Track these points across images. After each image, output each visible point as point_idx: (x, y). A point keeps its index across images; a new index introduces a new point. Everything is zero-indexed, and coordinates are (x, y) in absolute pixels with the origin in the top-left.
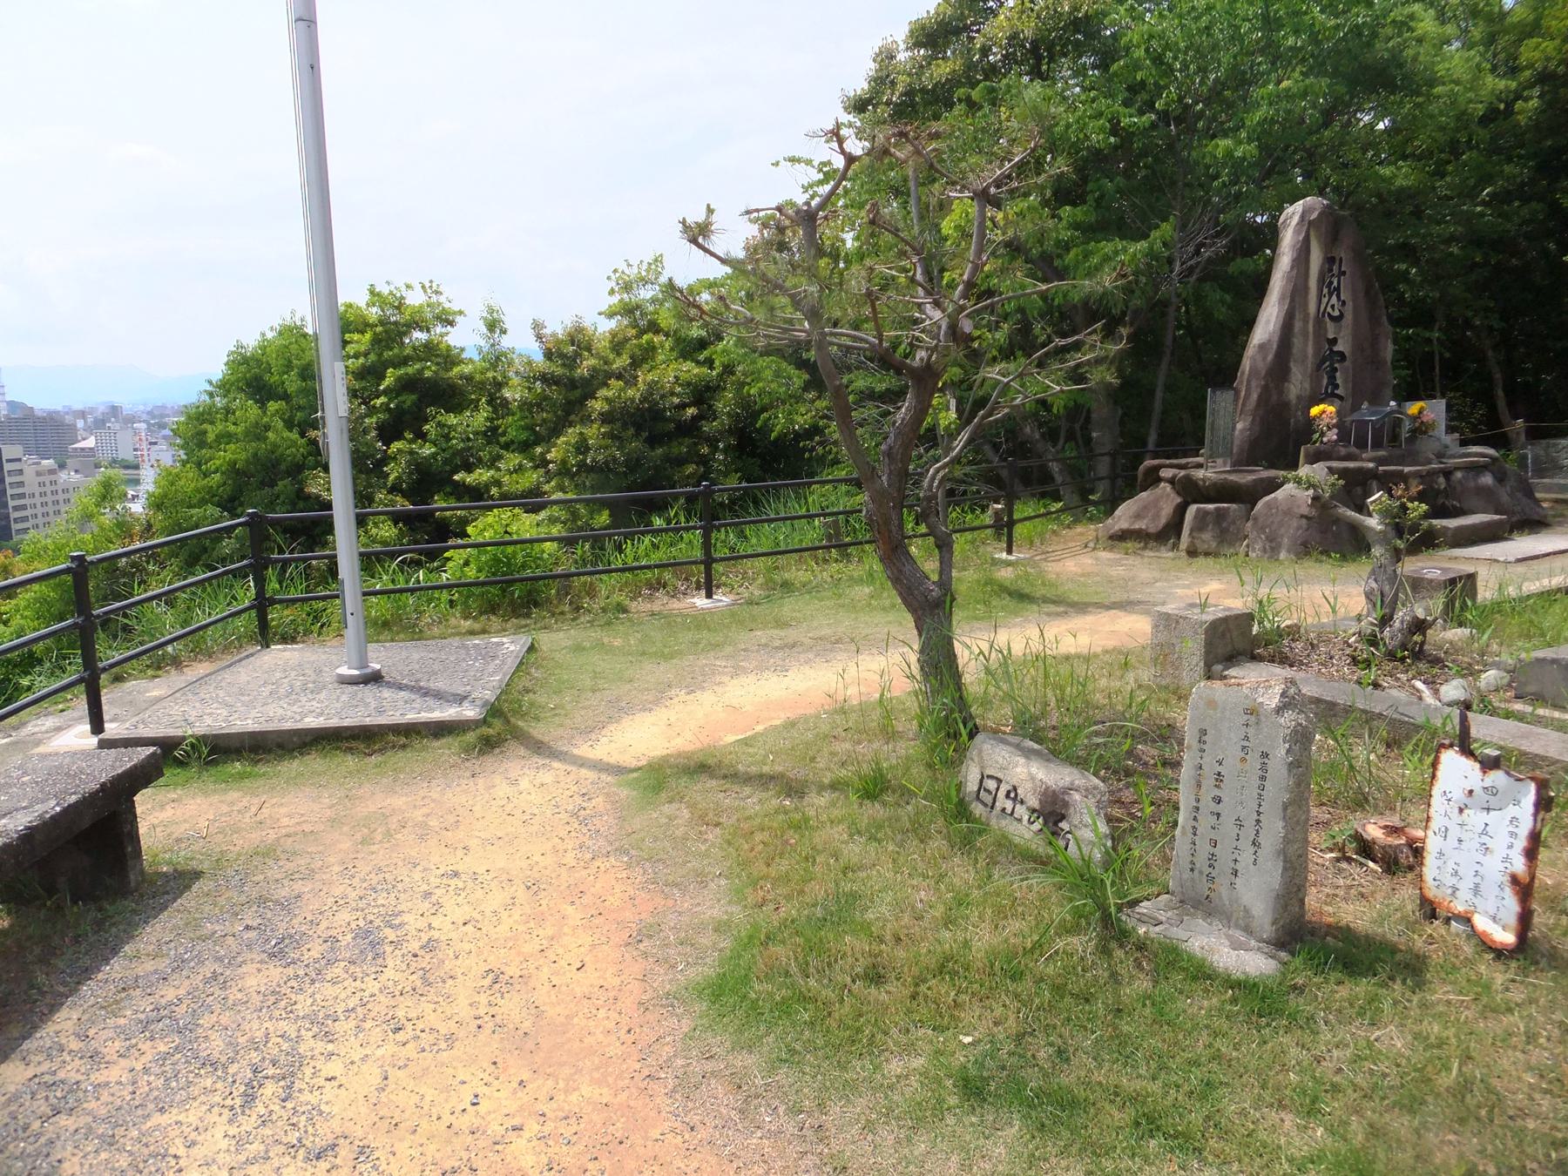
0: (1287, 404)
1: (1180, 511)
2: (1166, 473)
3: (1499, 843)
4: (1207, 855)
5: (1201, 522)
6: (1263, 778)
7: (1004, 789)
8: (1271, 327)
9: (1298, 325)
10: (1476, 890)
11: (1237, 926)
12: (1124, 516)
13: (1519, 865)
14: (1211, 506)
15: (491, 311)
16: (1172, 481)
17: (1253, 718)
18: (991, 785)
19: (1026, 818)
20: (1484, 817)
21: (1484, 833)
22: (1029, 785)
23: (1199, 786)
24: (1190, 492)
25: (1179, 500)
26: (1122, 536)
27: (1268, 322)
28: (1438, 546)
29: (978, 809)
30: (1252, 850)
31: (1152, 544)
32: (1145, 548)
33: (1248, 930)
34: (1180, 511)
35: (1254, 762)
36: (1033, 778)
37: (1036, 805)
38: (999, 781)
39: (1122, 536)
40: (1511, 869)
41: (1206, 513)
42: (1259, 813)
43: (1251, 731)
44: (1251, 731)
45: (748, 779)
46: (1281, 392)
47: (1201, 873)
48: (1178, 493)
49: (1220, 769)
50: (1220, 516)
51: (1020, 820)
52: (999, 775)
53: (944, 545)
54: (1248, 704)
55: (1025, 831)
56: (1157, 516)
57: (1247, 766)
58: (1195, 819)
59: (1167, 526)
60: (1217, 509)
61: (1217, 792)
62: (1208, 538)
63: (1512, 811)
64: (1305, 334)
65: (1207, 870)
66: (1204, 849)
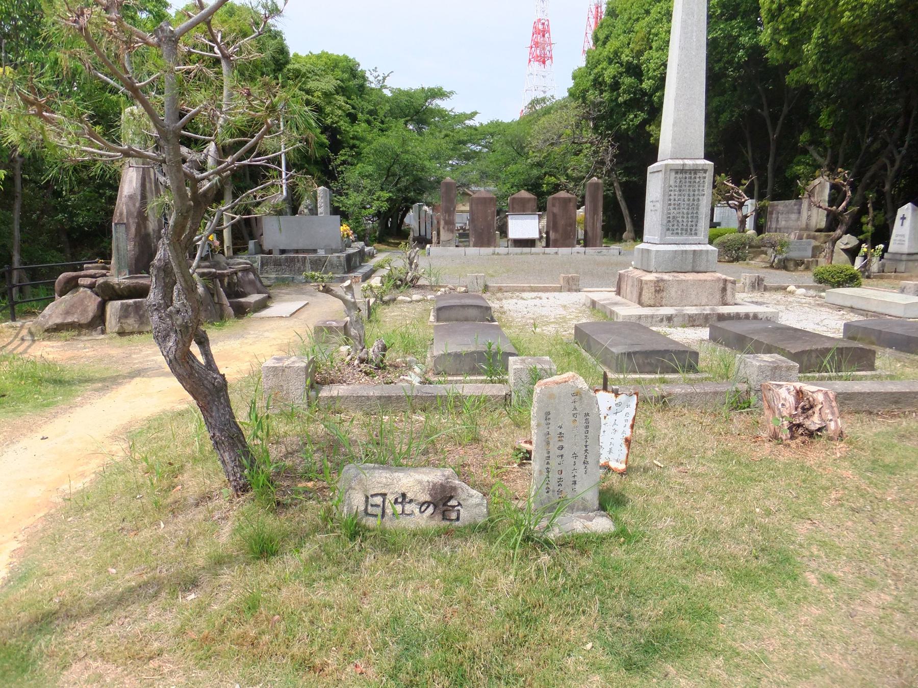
0: (148, 235)
1: (102, 308)
2: (81, 281)
3: (620, 428)
4: (557, 480)
5: (125, 313)
6: (587, 427)
7: (391, 498)
8: (134, 184)
9: (148, 185)
10: (610, 452)
11: (578, 510)
12: (53, 312)
13: (628, 433)
14: (131, 301)
15: (452, 93)
16: (91, 287)
17: (577, 397)
18: (378, 500)
19: (417, 511)
20: (615, 417)
21: (615, 424)
22: (418, 488)
23: (548, 443)
24: (109, 293)
25: (100, 299)
26: (57, 329)
27: (131, 181)
28: (247, 313)
29: (371, 522)
30: (583, 466)
31: (84, 331)
32: (79, 335)
33: (585, 509)
34: (102, 308)
35: (581, 420)
36: (420, 482)
37: (428, 498)
38: (384, 495)
39: (57, 329)
40: (626, 436)
41: (128, 306)
42: (586, 446)
43: (577, 404)
44: (577, 404)
45: (120, 601)
46: (145, 228)
47: (554, 491)
48: (97, 294)
49: (560, 430)
50: (137, 307)
51: (412, 513)
52: (383, 491)
53: (203, 343)
54: (574, 390)
55: (422, 519)
56: (85, 311)
57: (577, 424)
58: (548, 463)
59: (94, 318)
60: (135, 303)
61: (560, 444)
62: (131, 323)
63: (626, 410)
64: (151, 188)
65: (557, 489)
66: (554, 477)
